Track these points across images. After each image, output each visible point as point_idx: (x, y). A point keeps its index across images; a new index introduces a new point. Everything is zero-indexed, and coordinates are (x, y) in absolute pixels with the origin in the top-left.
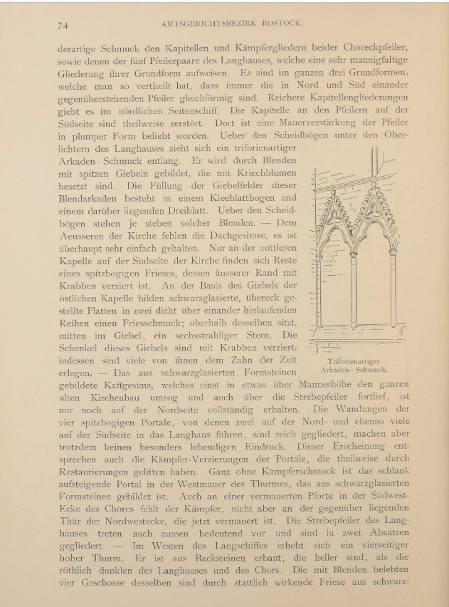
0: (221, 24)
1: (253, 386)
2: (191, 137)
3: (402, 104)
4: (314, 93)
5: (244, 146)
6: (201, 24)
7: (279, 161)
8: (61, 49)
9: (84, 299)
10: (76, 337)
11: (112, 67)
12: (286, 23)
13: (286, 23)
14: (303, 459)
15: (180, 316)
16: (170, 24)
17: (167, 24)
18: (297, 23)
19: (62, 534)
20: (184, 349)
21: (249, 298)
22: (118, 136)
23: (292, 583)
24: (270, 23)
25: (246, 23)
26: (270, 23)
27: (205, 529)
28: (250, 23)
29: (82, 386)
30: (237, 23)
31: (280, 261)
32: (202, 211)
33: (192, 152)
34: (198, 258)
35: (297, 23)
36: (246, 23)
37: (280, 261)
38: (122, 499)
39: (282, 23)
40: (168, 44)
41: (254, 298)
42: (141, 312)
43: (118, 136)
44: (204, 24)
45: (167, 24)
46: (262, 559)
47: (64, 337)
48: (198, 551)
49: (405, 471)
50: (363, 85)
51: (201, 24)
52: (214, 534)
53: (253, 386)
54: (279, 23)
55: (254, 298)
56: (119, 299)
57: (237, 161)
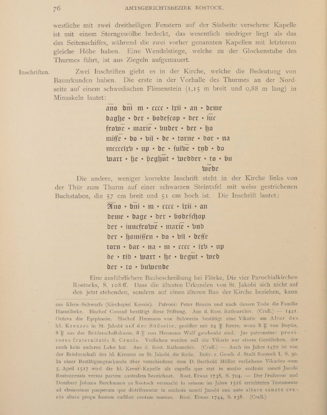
0: (167, 8)
2: (290, 80)
6: (153, 8)
8: (296, 292)
9: (260, 179)
12: (212, 8)
13: (212, 8)
14: (130, 333)
15: (92, 76)
16: (131, 8)
18: (219, 8)
19: (99, 81)
20: (136, 52)
21: (123, 119)
23: (75, 98)
24: (201, 8)
25: (183, 8)
26: (201, 8)
27: (72, 39)
30: (178, 8)
34: (189, 70)
36: (183, 8)
40: (276, 22)
42: (158, 43)
43: (160, 25)
44: (155, 8)
51: (153, 8)
52: (77, 43)
54: (207, 8)
57: (128, 237)
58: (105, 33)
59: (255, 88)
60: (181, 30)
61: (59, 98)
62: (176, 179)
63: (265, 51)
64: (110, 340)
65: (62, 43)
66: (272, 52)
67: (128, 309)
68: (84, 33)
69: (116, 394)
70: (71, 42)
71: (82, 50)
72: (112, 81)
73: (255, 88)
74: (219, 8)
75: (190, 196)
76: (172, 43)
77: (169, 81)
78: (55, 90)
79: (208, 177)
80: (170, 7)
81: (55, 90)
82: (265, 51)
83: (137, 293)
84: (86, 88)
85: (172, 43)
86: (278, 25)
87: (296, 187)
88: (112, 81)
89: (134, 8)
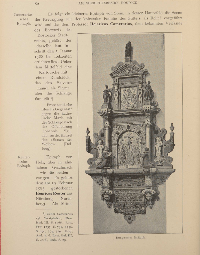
1: (52, 30)
3: (69, 64)
4: (40, 71)
5: (133, 17)
7: (67, 189)
10: (52, 67)
11: (46, 53)
12: (131, 3)
13: (131, 3)
17: (81, 3)
22: (61, 183)
23: (52, 36)
24: (125, 3)
28: (116, 3)
29: (44, 110)
30: (110, 3)
31: (20, 157)
32: (67, 204)
33: (55, 111)
35: (136, 3)
37: (153, 18)
38: (51, 41)
39: (130, 3)
41: (51, 163)
44: (96, 3)
45: (81, 3)
46: (62, 189)
47: (64, 73)
48: (56, 116)
49: (71, 183)
50: (50, 25)
53: (52, 30)
54: (128, 3)
55: (51, 163)
56: (48, 36)
58: (130, 18)
59: (41, 56)
60: (123, 16)
61: (48, 68)
62: (173, 13)
63: (117, 24)
64: (150, 18)
65: (125, 19)
66: (63, 78)
67: (102, 17)
68: (79, 13)
69: (126, 16)
70: (130, 18)
71: (37, 193)
72: (67, 173)
73: (41, 56)
74: (136, 3)
75: (47, 36)
76: (166, 19)
77: (121, 19)
78: (36, 25)
79: (52, 66)
80: (106, 3)
81: (36, 25)
82: (117, 24)
83: (85, 25)
84: (67, 13)
85: (166, 19)
86: (45, 19)
87: (29, 166)
88: (67, 173)
89: (84, 3)
